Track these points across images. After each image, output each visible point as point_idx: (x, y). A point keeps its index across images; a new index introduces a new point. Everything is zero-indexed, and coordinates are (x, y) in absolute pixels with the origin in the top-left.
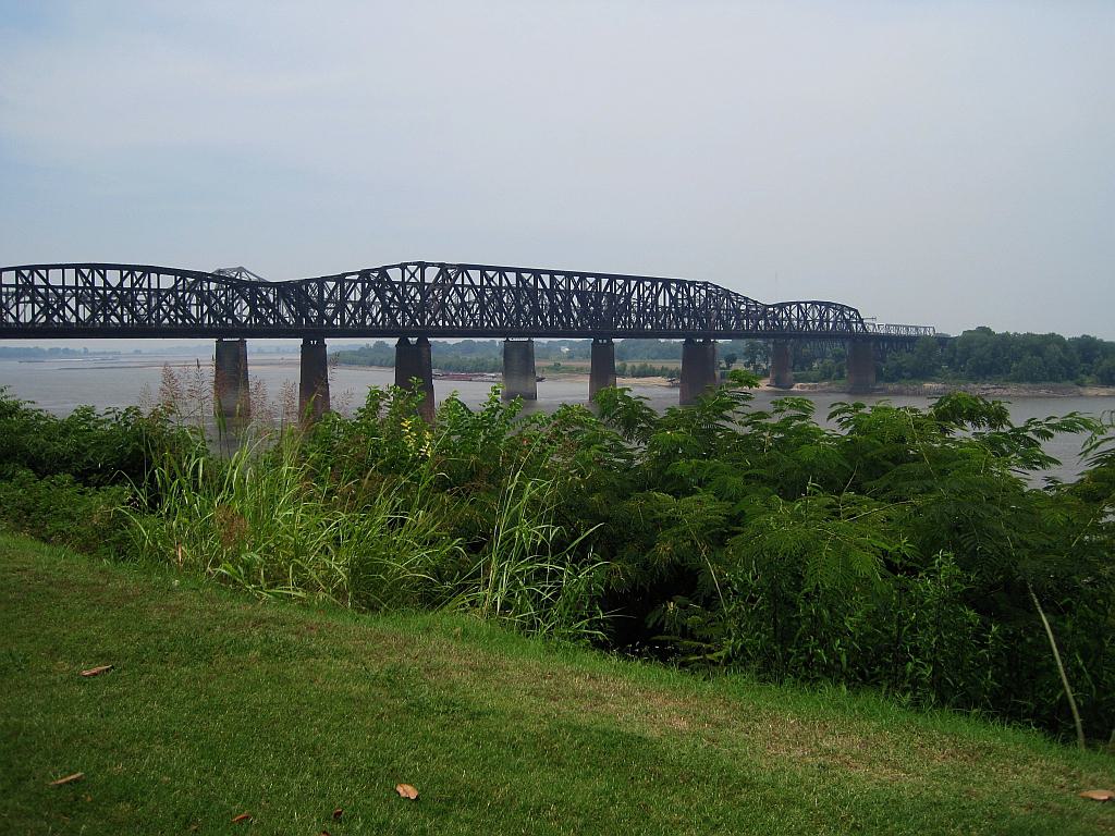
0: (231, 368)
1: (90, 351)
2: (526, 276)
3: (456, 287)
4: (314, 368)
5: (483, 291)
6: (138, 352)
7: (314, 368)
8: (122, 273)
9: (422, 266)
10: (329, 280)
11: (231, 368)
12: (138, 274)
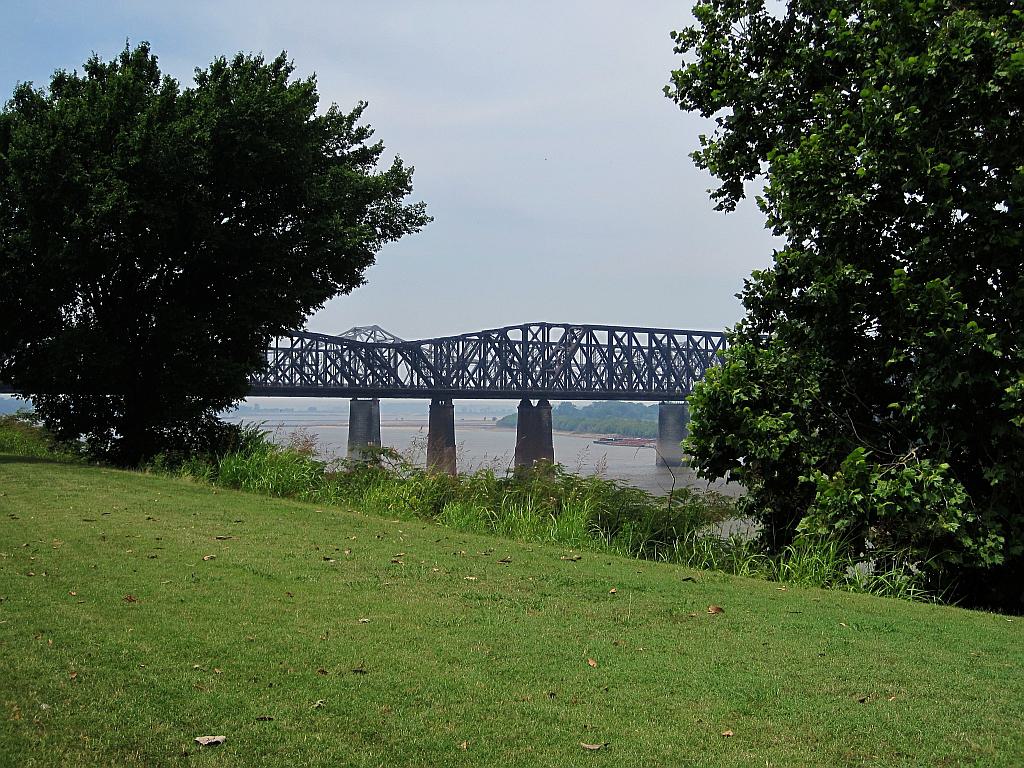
0: (364, 427)
1: (262, 408)
2: (659, 336)
3: (581, 346)
4: (442, 429)
5: (612, 353)
6: (312, 409)
7: (442, 429)
8: (292, 340)
9: (545, 327)
10: (636, 331)
11: (364, 427)
12: (307, 341)
